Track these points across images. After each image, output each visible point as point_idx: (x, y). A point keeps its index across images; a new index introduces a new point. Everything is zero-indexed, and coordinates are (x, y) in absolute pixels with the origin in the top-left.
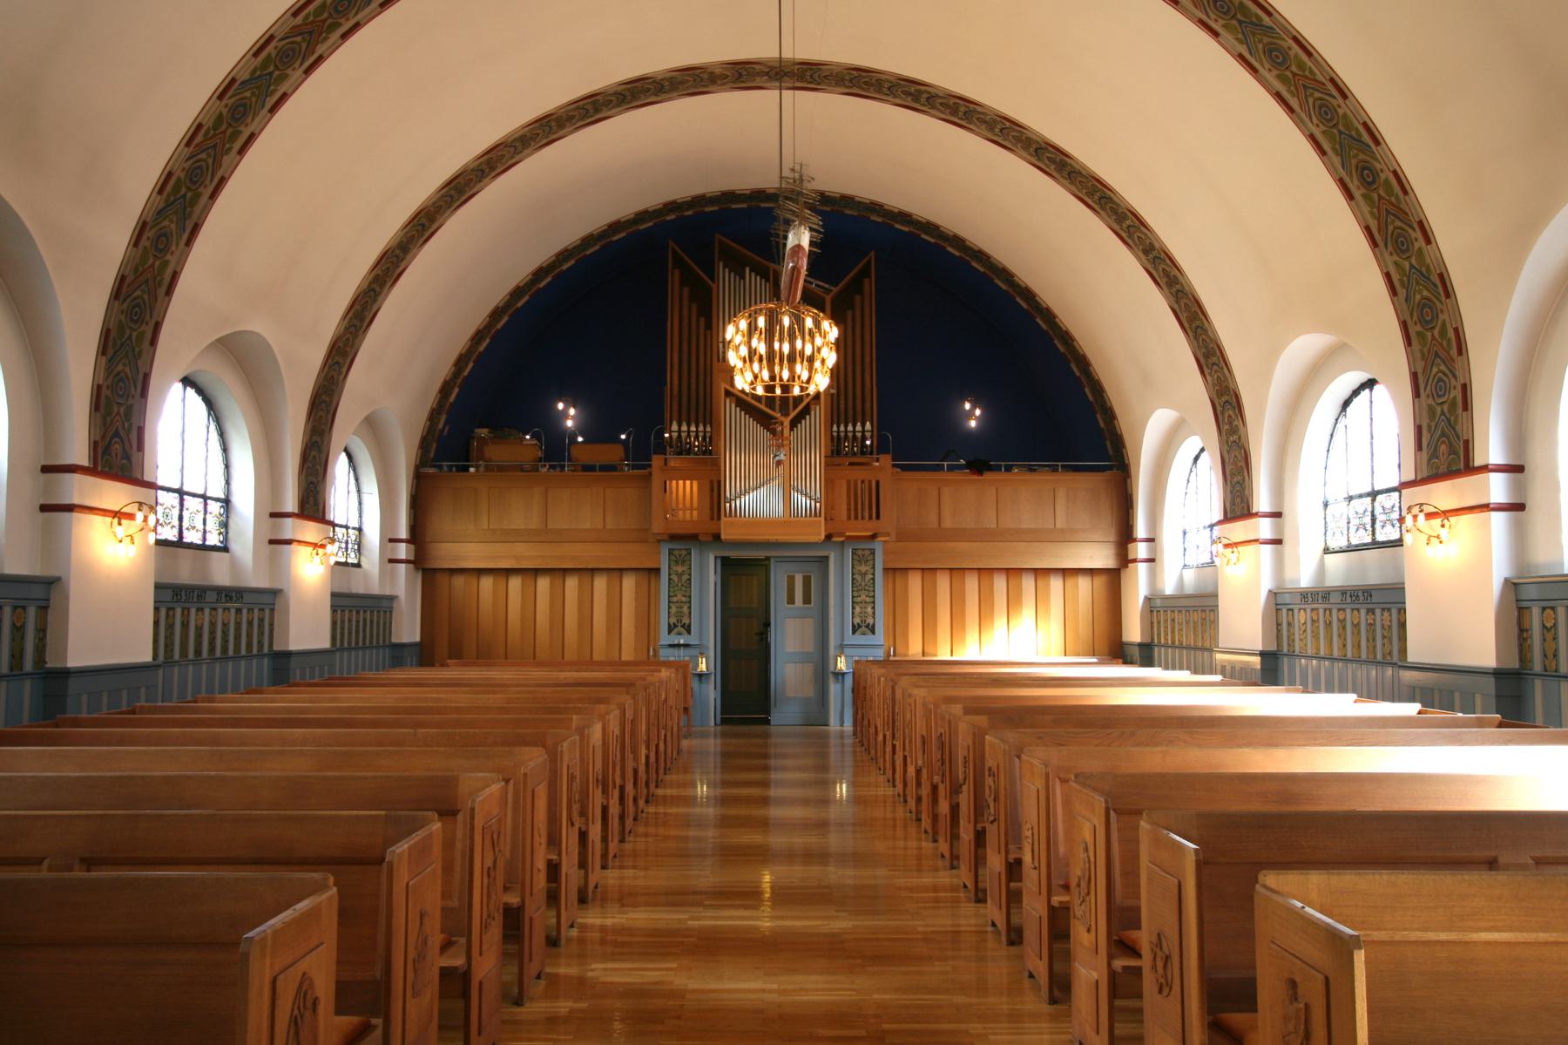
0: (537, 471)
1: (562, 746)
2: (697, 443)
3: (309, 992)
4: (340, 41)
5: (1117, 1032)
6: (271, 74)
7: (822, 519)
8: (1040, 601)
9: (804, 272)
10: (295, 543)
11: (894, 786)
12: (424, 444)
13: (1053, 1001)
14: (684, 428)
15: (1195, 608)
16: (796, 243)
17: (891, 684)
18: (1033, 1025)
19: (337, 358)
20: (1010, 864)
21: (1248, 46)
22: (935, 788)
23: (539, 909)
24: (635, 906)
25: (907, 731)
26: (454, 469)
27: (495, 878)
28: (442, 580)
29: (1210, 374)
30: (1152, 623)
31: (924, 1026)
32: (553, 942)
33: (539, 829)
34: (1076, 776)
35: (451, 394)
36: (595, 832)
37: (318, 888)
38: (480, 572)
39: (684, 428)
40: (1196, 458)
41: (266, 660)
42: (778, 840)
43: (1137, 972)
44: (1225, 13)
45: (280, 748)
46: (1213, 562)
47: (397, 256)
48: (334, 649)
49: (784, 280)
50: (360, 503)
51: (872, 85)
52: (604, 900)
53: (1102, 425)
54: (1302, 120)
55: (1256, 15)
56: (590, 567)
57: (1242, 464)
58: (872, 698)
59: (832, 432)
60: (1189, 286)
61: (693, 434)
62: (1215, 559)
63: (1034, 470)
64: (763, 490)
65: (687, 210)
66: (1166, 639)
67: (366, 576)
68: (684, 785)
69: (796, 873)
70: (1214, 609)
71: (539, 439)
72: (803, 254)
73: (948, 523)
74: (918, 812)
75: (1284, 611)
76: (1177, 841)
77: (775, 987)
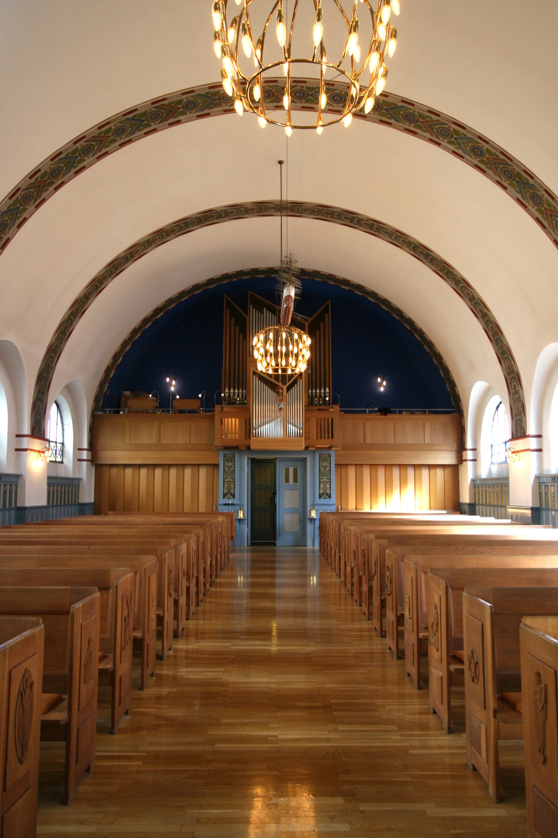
0: (155, 413)
1: (165, 555)
2: (238, 399)
3: (29, 678)
4: (54, 191)
5: (452, 704)
6: (18, 208)
7: (303, 438)
8: (417, 481)
9: (292, 309)
10: (28, 451)
11: (340, 577)
12: (97, 399)
13: (420, 688)
14: (232, 391)
15: (497, 485)
16: (288, 294)
17: (338, 524)
18: (410, 700)
19: (51, 355)
20: (398, 616)
21: (522, 194)
22: (360, 578)
23: (152, 639)
24: (203, 639)
25: (346, 548)
26: (112, 412)
27: (128, 623)
28: (106, 470)
29: (504, 363)
30: (475, 493)
31: (353, 701)
32: (159, 658)
33: (152, 598)
34: (431, 570)
35: (111, 373)
36: (183, 600)
37: (37, 624)
38: (125, 466)
39: (232, 391)
40: (498, 407)
41: (13, 511)
42: (279, 605)
43: (462, 671)
44: (510, 177)
45: (18, 555)
46: (506, 461)
47: (83, 302)
48: (49, 506)
49: (282, 313)
50: (63, 430)
51: (329, 214)
52: (187, 636)
53: (449, 390)
54: (550, 233)
55: (526, 179)
56: (182, 463)
57: (521, 410)
58: (328, 532)
59: (308, 393)
60: (493, 318)
61: (236, 394)
62: (507, 459)
63: (414, 413)
64: (272, 424)
65: (234, 278)
66: (482, 501)
67: (66, 468)
68: (231, 577)
69: (290, 622)
70: (507, 485)
71: (157, 397)
72: (291, 300)
73: (369, 441)
74: (352, 591)
75: (543, 487)
76: (481, 602)
77: (275, 680)
